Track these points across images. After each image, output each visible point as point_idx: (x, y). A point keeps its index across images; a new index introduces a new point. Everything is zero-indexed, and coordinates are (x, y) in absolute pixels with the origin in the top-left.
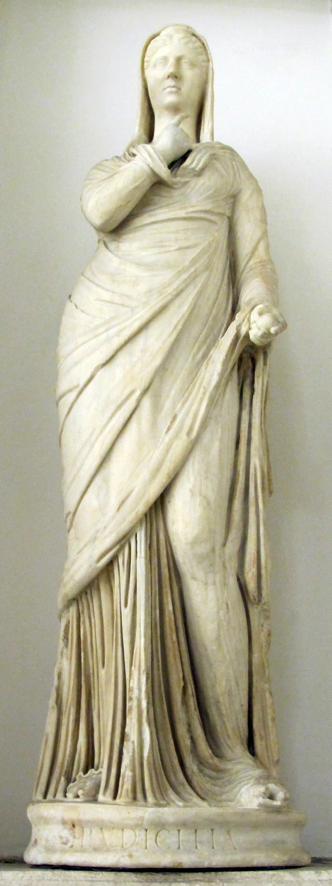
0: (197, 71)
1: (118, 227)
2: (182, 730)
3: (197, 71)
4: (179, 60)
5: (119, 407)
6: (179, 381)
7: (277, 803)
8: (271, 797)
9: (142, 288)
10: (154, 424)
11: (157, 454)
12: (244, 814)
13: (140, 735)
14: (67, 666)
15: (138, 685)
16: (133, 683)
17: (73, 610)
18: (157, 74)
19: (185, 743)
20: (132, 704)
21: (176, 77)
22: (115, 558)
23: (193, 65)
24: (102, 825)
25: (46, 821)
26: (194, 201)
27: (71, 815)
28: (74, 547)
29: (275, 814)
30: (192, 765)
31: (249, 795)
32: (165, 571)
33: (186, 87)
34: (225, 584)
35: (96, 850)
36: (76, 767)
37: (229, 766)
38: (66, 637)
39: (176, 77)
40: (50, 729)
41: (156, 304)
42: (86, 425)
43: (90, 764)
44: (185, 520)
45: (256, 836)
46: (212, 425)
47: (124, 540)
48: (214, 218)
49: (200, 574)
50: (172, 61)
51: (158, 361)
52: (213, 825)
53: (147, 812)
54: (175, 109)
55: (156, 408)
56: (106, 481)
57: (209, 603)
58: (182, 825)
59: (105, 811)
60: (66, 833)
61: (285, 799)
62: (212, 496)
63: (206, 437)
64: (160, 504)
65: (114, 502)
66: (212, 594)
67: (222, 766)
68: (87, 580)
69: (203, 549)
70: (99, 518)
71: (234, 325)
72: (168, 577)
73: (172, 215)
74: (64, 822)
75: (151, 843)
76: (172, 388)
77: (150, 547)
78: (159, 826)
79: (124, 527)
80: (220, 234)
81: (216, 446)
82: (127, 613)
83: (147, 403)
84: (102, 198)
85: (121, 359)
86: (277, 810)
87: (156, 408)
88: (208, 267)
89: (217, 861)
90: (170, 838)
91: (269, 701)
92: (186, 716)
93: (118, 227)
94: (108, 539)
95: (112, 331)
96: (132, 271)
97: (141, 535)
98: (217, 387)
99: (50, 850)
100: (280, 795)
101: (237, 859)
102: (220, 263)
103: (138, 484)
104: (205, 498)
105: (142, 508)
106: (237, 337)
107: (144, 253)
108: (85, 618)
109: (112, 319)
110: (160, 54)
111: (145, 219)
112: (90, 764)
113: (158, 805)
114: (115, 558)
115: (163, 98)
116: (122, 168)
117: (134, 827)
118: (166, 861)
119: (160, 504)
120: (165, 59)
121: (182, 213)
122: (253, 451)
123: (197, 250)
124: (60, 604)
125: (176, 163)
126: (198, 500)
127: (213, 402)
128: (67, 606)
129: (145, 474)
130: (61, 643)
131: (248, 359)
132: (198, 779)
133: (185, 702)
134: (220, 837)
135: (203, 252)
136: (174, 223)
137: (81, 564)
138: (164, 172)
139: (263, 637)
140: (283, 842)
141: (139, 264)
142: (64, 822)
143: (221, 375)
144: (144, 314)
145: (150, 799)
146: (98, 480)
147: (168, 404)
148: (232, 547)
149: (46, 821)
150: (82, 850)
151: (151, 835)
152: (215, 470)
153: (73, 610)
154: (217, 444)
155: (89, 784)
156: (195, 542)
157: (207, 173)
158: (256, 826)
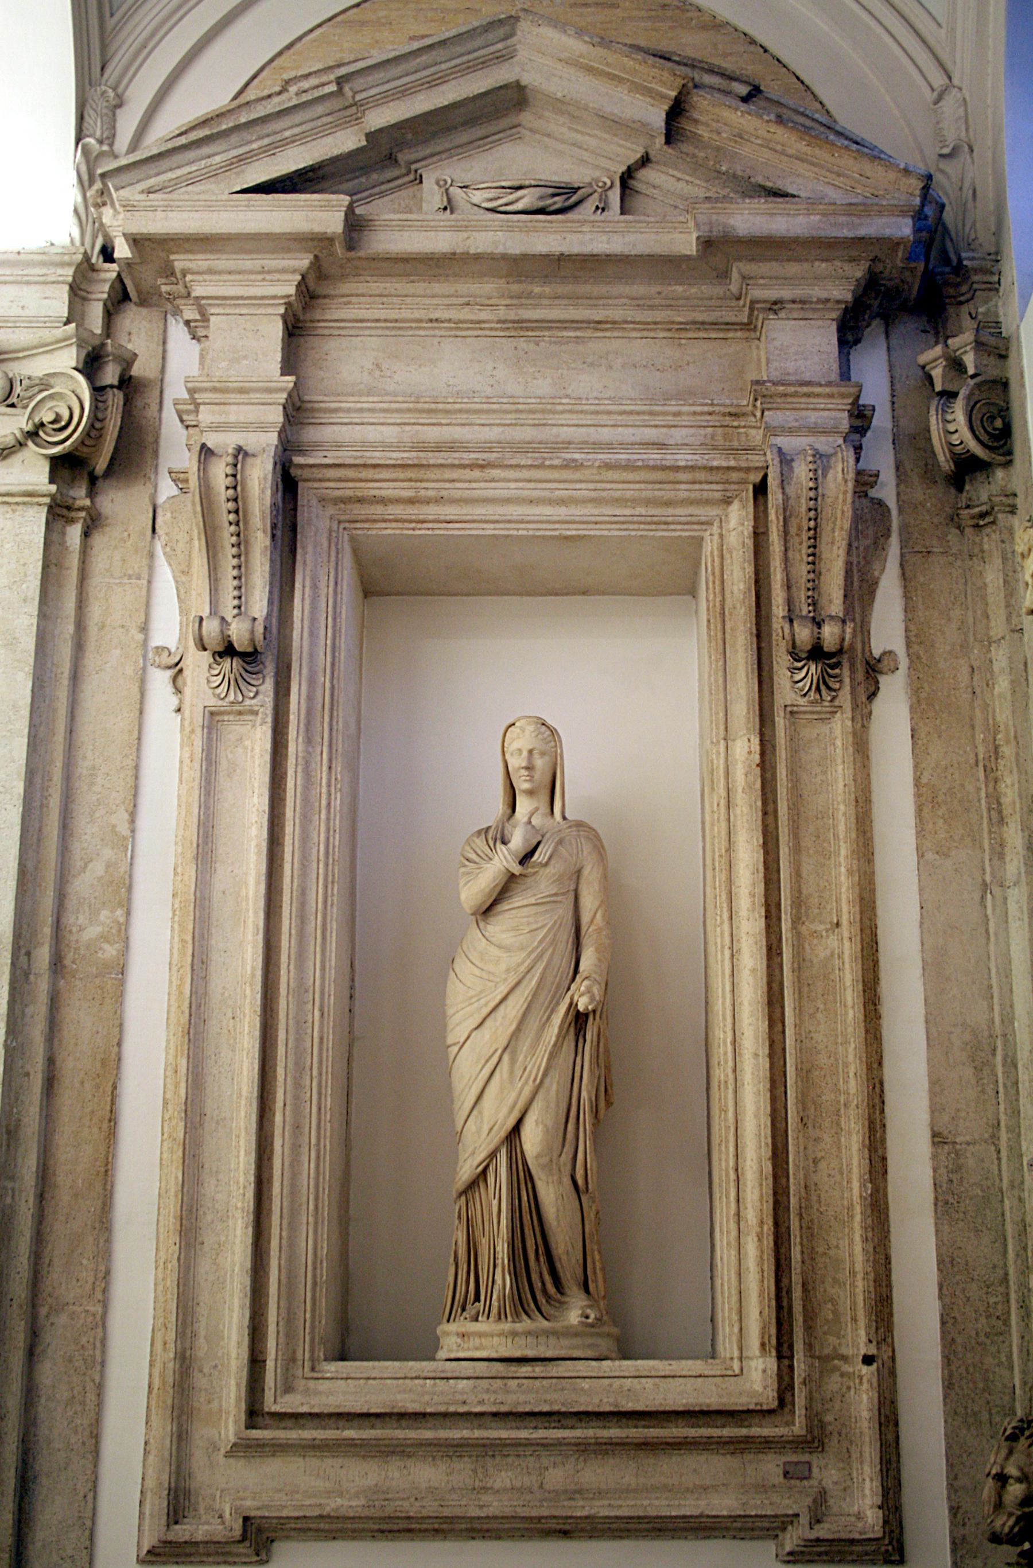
0: (547, 758)
1: (487, 911)
2: (535, 1276)
3: (547, 758)
4: (531, 752)
5: (487, 1061)
6: (529, 1040)
7: (590, 1321)
8: (587, 1317)
9: (503, 967)
10: (511, 1072)
11: (513, 1095)
12: (571, 1326)
13: (503, 1281)
14: (461, 1237)
15: (503, 1250)
16: (499, 1249)
17: (463, 1198)
18: (515, 763)
19: (538, 1285)
20: (499, 1262)
21: (529, 768)
22: (487, 1166)
23: (543, 754)
24: (480, 1335)
25: (448, 1334)
26: (542, 886)
27: (462, 1330)
28: (463, 1156)
29: (589, 1328)
30: (542, 1300)
31: (573, 1317)
32: (521, 1174)
33: (537, 775)
34: (560, 1182)
35: (477, 1349)
36: (469, 1300)
37: (567, 1299)
38: (459, 1217)
39: (529, 768)
40: (451, 1279)
41: (512, 980)
42: (467, 1069)
43: (477, 1299)
44: (532, 1139)
45: (576, 1341)
46: (552, 1073)
47: (493, 1155)
48: (559, 898)
49: (544, 1177)
50: (525, 753)
51: (514, 1027)
52: (548, 1333)
53: (507, 1326)
54: (530, 793)
55: (513, 1061)
56: (480, 1113)
57: (552, 1194)
58: (528, 1333)
59: (482, 1326)
60: (459, 1340)
61: (596, 1318)
62: (550, 1124)
63: (548, 1081)
64: (516, 1129)
65: (486, 1128)
66: (552, 1190)
67: (564, 1299)
68: (470, 1180)
69: (545, 1160)
70: (478, 1139)
71: (570, 993)
72: (523, 1178)
73: (525, 902)
74: (458, 1334)
75: (509, 1344)
76: (525, 1045)
77: (510, 1158)
78: (514, 1334)
79: (492, 1147)
80: (564, 911)
81: (555, 1086)
82: (495, 1202)
83: (506, 1058)
84: (475, 888)
85: (488, 1023)
86: (592, 1326)
87: (513, 1061)
88: (554, 942)
89: (549, 1354)
90: (521, 1341)
91: (597, 1257)
92: (538, 1269)
93: (487, 911)
94: (482, 1155)
95: (483, 1002)
96: (495, 952)
97: (504, 1151)
98: (555, 1045)
99: (450, 1351)
100: (592, 1316)
101: (563, 1353)
102: (566, 935)
103: (501, 1116)
104: (545, 1126)
105: (503, 1134)
106: (571, 1004)
107: (504, 936)
108: (471, 1204)
109: (481, 992)
110: (515, 745)
111: (504, 906)
112: (477, 1299)
113: (513, 1322)
114: (487, 1166)
115: (522, 784)
116: (363, 1502)
117: (499, 1335)
118: (518, 1354)
119: (516, 1129)
120: (520, 750)
121: (533, 901)
122: (583, 1087)
123: (545, 930)
124: (454, 1195)
125: (526, 858)
126: (541, 1127)
127: (553, 1056)
128: (460, 1195)
129: (504, 1110)
130: (457, 1222)
131: (579, 1020)
132: (545, 1307)
133: (537, 1259)
134: (552, 1340)
135: (550, 930)
136: (525, 909)
137: (466, 1171)
138: (517, 869)
139: (592, 1215)
140: (598, 1346)
141: (499, 947)
142: (458, 1334)
143: (558, 1037)
144: (503, 989)
145: (509, 1319)
146: (475, 1112)
147: (521, 1058)
148: (566, 1157)
149: (448, 1334)
150: (469, 1349)
151: (510, 1340)
152: (553, 1105)
153: (463, 1198)
154: (555, 1086)
155: (474, 1312)
156: (537, 1157)
157: (553, 862)
158: (576, 1335)
